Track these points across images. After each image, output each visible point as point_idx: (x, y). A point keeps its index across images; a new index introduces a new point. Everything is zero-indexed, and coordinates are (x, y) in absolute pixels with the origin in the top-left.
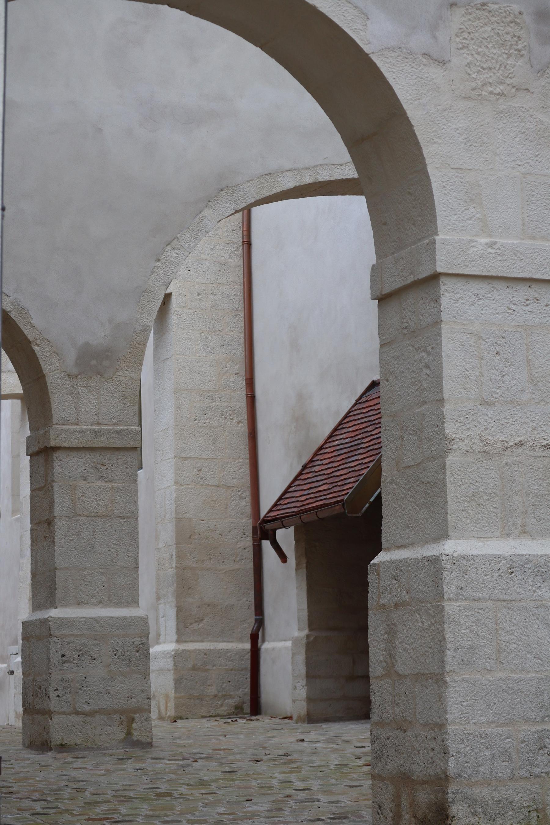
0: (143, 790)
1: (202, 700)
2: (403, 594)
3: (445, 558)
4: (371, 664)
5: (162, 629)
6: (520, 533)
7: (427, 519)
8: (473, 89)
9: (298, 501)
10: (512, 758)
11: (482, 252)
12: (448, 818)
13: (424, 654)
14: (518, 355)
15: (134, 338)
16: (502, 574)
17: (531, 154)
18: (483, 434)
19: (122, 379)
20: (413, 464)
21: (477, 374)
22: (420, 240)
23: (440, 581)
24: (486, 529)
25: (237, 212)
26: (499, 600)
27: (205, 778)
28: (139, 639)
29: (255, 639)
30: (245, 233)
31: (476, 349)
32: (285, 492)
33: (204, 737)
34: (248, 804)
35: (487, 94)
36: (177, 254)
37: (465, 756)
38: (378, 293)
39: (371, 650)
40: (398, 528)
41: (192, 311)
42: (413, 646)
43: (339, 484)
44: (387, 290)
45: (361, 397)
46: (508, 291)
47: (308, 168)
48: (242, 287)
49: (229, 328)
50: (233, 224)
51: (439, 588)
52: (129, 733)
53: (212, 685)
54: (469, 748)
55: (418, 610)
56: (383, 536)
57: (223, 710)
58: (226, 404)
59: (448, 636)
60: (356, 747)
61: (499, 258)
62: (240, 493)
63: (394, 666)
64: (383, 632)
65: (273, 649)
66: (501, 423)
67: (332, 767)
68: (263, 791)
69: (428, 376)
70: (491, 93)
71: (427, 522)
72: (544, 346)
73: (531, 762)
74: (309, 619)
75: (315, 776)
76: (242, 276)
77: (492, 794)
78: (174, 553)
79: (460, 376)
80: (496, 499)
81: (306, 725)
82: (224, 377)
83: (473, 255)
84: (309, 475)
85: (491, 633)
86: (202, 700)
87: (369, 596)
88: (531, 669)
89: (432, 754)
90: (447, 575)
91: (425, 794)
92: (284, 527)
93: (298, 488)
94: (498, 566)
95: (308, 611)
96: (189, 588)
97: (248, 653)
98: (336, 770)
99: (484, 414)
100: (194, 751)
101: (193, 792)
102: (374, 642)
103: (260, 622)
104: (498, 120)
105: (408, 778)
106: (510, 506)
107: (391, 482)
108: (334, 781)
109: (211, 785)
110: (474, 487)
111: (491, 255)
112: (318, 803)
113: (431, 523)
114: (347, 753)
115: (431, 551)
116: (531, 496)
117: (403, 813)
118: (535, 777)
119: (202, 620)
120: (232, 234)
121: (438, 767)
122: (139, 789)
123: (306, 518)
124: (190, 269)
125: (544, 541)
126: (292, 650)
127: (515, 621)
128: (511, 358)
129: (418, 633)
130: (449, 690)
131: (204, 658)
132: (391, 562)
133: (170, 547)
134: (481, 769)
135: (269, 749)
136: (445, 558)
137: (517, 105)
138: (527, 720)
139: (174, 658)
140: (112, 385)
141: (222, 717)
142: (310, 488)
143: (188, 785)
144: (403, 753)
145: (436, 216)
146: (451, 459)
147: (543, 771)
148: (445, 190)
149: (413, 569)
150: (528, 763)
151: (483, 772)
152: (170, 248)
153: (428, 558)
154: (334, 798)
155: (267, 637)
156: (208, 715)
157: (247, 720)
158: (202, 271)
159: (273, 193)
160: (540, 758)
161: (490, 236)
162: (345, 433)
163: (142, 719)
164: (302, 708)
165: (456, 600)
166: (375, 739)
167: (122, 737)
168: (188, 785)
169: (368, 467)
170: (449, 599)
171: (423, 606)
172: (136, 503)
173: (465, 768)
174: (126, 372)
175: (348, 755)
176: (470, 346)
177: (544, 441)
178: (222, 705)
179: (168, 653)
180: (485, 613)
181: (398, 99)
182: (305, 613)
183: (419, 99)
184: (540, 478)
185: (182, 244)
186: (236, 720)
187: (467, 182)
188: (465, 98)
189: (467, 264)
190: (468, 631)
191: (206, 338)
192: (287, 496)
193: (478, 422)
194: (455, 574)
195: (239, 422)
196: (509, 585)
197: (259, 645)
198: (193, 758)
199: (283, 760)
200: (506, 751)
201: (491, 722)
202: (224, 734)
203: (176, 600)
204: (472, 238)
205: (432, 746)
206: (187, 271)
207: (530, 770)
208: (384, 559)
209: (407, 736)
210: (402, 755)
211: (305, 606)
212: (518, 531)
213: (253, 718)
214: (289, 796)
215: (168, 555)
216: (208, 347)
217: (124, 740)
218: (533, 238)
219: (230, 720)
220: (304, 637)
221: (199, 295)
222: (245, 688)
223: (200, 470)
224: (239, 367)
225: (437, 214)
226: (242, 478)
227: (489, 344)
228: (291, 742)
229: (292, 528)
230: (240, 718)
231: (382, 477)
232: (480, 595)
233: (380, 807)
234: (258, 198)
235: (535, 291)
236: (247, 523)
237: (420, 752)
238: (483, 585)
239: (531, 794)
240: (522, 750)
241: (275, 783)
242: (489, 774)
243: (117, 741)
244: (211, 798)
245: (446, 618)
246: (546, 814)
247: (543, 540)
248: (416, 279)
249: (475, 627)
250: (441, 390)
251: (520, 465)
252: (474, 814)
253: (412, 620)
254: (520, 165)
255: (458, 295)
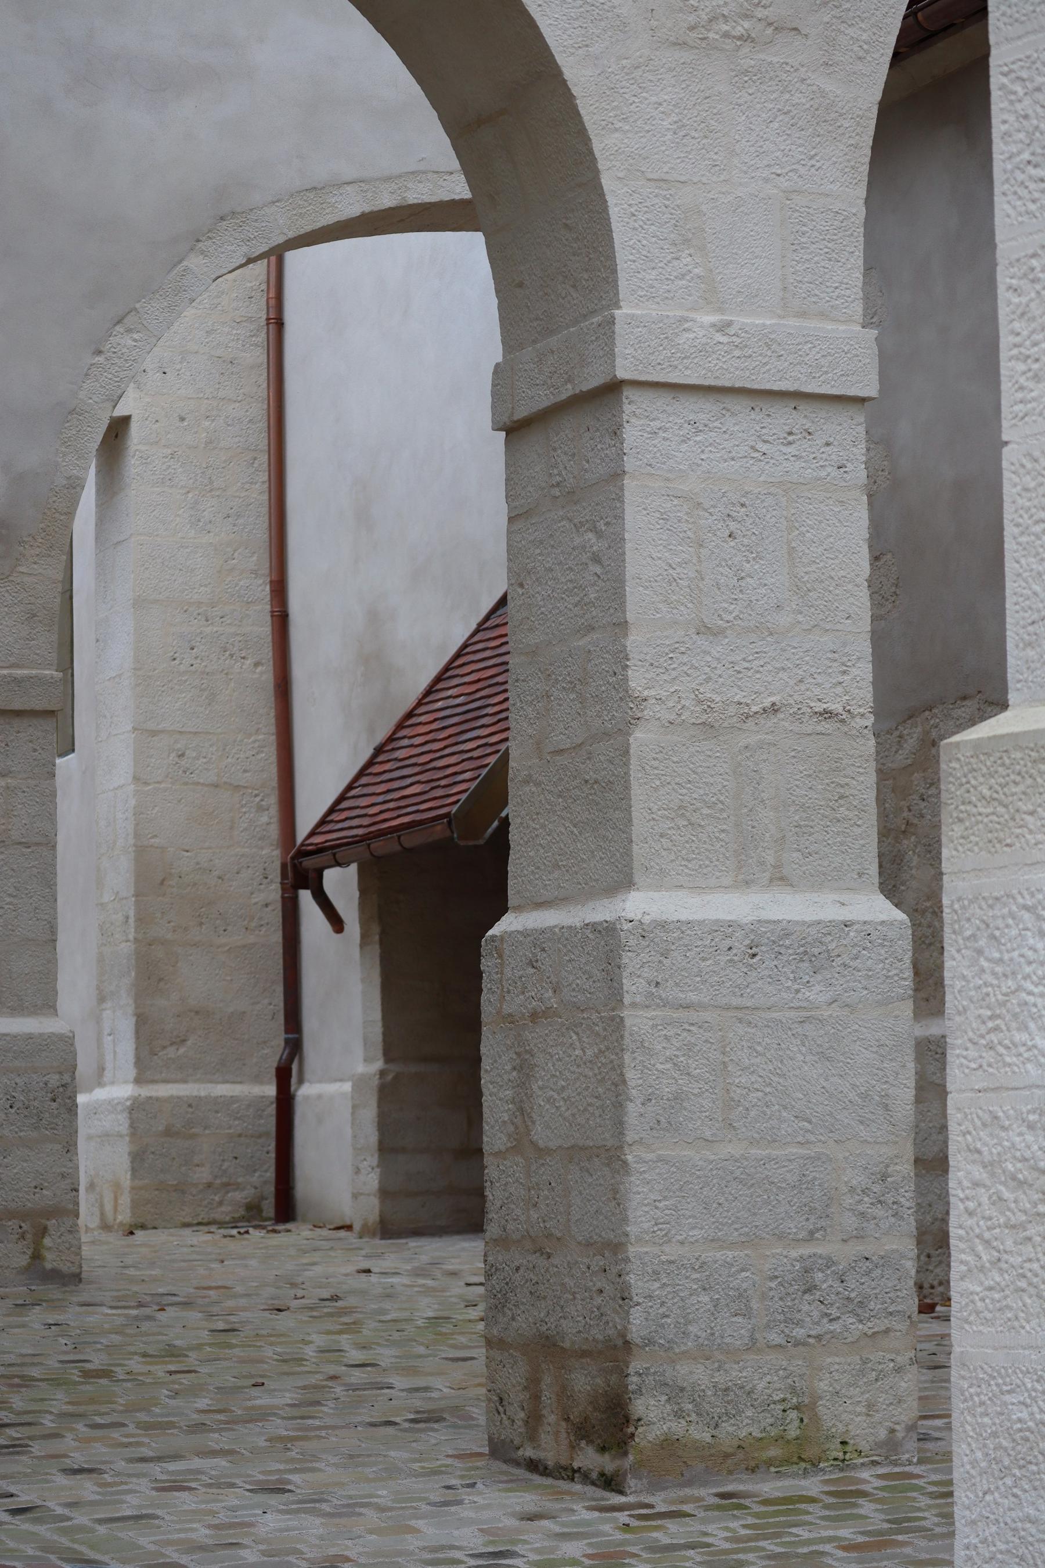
0: (57, 1365)
1: (183, 1192)
2: (546, 995)
3: (627, 926)
4: (486, 1127)
5: (109, 1057)
6: (771, 880)
7: (593, 852)
8: (692, 28)
9: (365, 815)
10: (751, 1309)
11: (704, 340)
12: (628, 1421)
13: (585, 1110)
14: (770, 539)
15: (51, 501)
16: (735, 958)
17: (801, 153)
18: (702, 690)
19: (26, 579)
20: (567, 746)
21: (692, 575)
22: (585, 316)
23: (617, 971)
24: (705, 871)
25: (250, 261)
26: (728, 1008)
27: (178, 1343)
28: (57, 1077)
29: (284, 1077)
30: (272, 302)
31: (690, 526)
32: (342, 798)
33: (183, 1264)
34: (255, 1392)
35: (717, 37)
36: (135, 340)
37: (663, 1304)
38: (505, 419)
39: (487, 1100)
40: (538, 868)
41: (169, 451)
42: (564, 1095)
43: (443, 783)
44: (521, 413)
45: (487, 618)
46: (753, 417)
47: (388, 179)
48: (266, 407)
49: (239, 484)
50: (249, 285)
51: (615, 984)
52: (37, 1256)
53: (203, 1165)
54: (669, 1289)
55: (575, 1026)
56: (510, 883)
57: (224, 1212)
58: (232, 630)
59: (630, 1075)
60: (468, 1285)
61: (737, 353)
62: (258, 799)
63: (528, 1132)
64: (508, 1067)
65: (320, 1097)
66: (736, 668)
67: (420, 1323)
68: (285, 1368)
69: (599, 577)
70: (726, 35)
71: (594, 857)
72: (820, 522)
73: (788, 1315)
74: (384, 1041)
75: (387, 1340)
76: (265, 385)
77: (713, 1377)
78: (132, 913)
79: (658, 579)
80: (725, 815)
81: (377, 1242)
82: (230, 578)
83: (686, 347)
84: (387, 766)
85: (714, 1070)
86: (183, 1192)
87: (484, 997)
88: (789, 1139)
89: (598, 1300)
90: (630, 959)
91: (586, 1376)
92: (339, 864)
93: (366, 791)
94: (728, 942)
95: (384, 1026)
96: (161, 980)
97: (272, 1103)
98: (427, 1327)
99: (704, 652)
100: (161, 1290)
101: (152, 1368)
102: (491, 1087)
103: (295, 1046)
104: (738, 88)
105: (555, 1345)
106: (753, 827)
107: (526, 782)
108: (422, 1350)
109: (187, 1356)
110: (684, 791)
111: (721, 347)
112: (387, 1391)
113: (601, 858)
114: (451, 1297)
115: (599, 912)
116: (792, 809)
117: (544, 1412)
118: (795, 1346)
119: (184, 1041)
120: (247, 303)
121: (611, 1325)
122: (50, 1362)
123: (379, 847)
124: (166, 370)
125: (816, 895)
126: (352, 1098)
127: (759, 1048)
128: (757, 544)
129: (574, 1068)
130: (632, 1179)
131: (187, 1112)
132: (525, 933)
133: (124, 901)
134: (693, 1329)
135: (303, 1286)
136: (627, 926)
137: (775, 60)
138: (781, 1237)
139: (130, 1113)
140: (7, 591)
141: (221, 1224)
142: (389, 791)
143: (145, 1355)
144: (545, 1298)
145: (616, 271)
146: (639, 737)
147: (812, 1333)
148: (635, 221)
149: (565, 946)
150: (781, 1317)
151: (696, 1336)
152: (122, 330)
153: (594, 927)
154: (420, 1382)
155: (307, 1075)
156: (195, 1222)
157: (268, 1232)
158: (189, 374)
159: (319, 225)
160: (806, 1308)
161: (721, 310)
162: (457, 686)
163: (62, 1229)
164: (370, 1209)
165: (647, 1007)
166: (493, 1270)
167: (24, 1263)
168: (145, 1355)
169: (498, 751)
170: (634, 1005)
171: (583, 1018)
172: (51, 817)
173: (662, 1326)
174: (35, 566)
175: (453, 1300)
176: (679, 521)
177: (820, 704)
178: (221, 1203)
179: (118, 1104)
180: (701, 1031)
181: (547, 45)
182: (377, 1030)
183: (587, 46)
184: (810, 776)
185: (145, 322)
186: (247, 1232)
187: (678, 206)
188: (675, 44)
189: (676, 363)
190: (668, 1066)
191: (196, 503)
192: (345, 804)
193: (693, 667)
194: (644, 957)
195: (257, 664)
196: (749, 980)
197: (293, 1088)
198: (158, 1304)
199: (329, 1308)
200: (740, 1295)
201: (712, 1241)
202: (221, 1257)
203: (135, 1002)
204: (686, 314)
205: (599, 1285)
206: (159, 375)
207: (787, 1331)
208: (513, 928)
209: (553, 1265)
210: (543, 1302)
211: (377, 1015)
212: (767, 875)
213: (281, 1227)
214: (333, 1378)
215: (120, 917)
216: (199, 521)
217: (27, 1269)
218: (803, 314)
219: (234, 1232)
220: (375, 1075)
221: (182, 419)
222: (266, 1171)
223: (183, 755)
224: (259, 559)
225: (619, 267)
226: (262, 771)
227: (715, 517)
228: (346, 1275)
229: (353, 868)
230: (255, 1227)
231: (510, 771)
232: (693, 997)
233: (501, 1399)
234: (291, 235)
235: (805, 416)
236: (272, 856)
237: (578, 1296)
238: (699, 979)
239: (787, 1377)
240: (771, 1293)
241: (309, 1351)
242: (708, 1339)
243: (14, 1271)
244: (185, 1380)
245: (627, 1041)
246: (816, 1415)
247: (814, 894)
248: (577, 392)
249: (682, 1059)
250: (623, 604)
251: (772, 749)
252: (679, 1414)
253: (563, 1044)
254: (779, 175)
255: (657, 424)
